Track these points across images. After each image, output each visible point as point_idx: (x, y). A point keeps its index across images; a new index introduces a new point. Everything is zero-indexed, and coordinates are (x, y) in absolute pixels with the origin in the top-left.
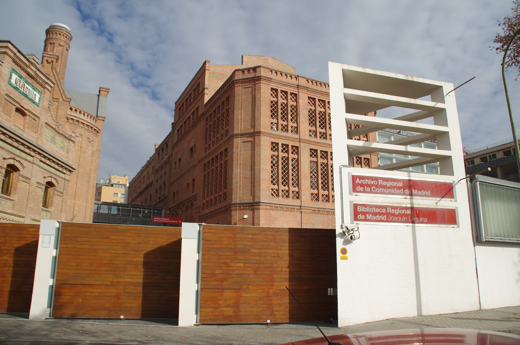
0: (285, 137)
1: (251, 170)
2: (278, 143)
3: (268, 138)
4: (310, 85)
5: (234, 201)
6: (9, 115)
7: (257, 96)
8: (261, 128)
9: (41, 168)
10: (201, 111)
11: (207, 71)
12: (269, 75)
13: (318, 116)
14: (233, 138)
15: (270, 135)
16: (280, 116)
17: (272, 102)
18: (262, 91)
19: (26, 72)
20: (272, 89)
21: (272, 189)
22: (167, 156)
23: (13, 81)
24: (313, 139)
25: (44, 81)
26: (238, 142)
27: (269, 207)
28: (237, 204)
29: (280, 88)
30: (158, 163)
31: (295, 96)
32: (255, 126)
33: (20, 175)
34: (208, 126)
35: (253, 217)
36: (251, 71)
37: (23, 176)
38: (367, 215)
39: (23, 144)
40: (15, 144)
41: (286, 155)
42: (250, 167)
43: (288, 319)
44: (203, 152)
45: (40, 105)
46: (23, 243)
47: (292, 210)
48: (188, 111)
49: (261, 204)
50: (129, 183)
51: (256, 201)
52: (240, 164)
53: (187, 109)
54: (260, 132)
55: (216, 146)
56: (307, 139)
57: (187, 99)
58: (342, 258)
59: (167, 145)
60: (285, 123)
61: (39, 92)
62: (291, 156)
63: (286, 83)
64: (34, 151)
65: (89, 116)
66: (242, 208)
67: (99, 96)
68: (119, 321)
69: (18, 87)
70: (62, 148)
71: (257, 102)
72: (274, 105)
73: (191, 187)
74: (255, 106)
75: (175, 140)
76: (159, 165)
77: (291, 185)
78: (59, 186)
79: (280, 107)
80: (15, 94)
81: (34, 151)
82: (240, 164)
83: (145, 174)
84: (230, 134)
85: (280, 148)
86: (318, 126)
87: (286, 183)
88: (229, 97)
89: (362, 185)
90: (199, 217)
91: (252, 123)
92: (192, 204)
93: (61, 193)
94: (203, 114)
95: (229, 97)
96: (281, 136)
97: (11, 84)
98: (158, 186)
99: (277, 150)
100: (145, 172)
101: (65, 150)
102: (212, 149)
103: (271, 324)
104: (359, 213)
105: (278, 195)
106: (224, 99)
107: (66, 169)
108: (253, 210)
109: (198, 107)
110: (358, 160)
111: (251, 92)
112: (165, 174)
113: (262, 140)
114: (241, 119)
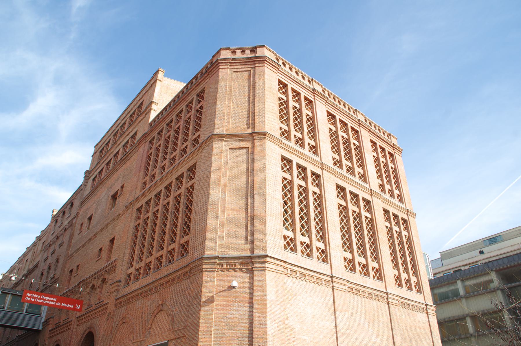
5: (208, 253)
7: (258, 83)
11: (158, 82)
18: (266, 77)
27: (281, 269)
28: (215, 258)
30: (53, 234)
47: (319, 281)
48: (117, 144)
49: (268, 259)
52: (225, 185)
66: (225, 266)
73: (104, 254)
74: (254, 96)
76: (54, 235)
82: (225, 185)
83: (29, 256)
92: (104, 280)
94: (146, 135)
100: (30, 254)
108: (251, 272)
111: (247, 77)
112: (61, 245)
113: (267, 146)
114: (229, 114)
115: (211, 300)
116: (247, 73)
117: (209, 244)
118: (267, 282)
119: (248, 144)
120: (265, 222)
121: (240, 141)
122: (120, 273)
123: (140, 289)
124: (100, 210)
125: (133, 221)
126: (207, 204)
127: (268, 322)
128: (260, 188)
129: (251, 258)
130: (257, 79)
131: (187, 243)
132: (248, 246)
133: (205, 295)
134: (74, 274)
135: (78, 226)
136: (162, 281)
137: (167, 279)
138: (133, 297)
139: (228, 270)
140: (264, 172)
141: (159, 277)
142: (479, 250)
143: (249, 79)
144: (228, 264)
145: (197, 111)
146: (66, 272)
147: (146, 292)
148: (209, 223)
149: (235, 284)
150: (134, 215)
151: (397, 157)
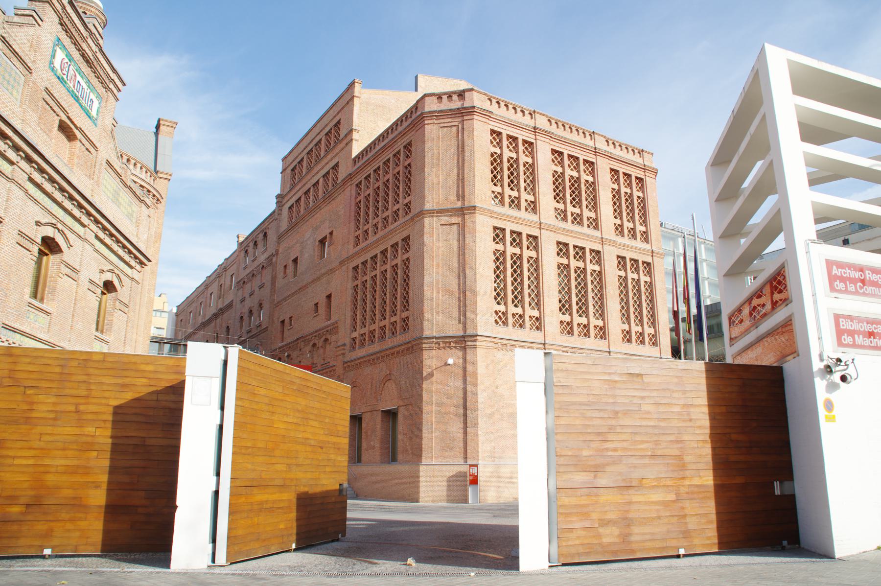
0: (516, 218)
1: (459, 276)
2: (504, 229)
3: (488, 219)
4: (553, 128)
5: (426, 334)
6: (48, 132)
7: (468, 142)
8: (476, 201)
9: (97, 251)
10: (342, 174)
12: (486, 105)
13: (568, 184)
14: (423, 218)
15: (491, 214)
16: (506, 181)
17: (492, 155)
18: (476, 133)
19: (80, 49)
20: (493, 132)
21: (496, 312)
22: (266, 255)
23: (57, 64)
24: (562, 225)
25: (108, 75)
26: (431, 224)
27: (493, 345)
28: (433, 338)
29: (506, 131)
30: (245, 268)
31: (529, 145)
32: (464, 196)
33: (63, 262)
34: (362, 198)
35: (465, 363)
36: (455, 97)
37: (68, 266)
38: (856, 336)
39: (71, 198)
40: (58, 195)
41: (517, 251)
42: (456, 271)
43: (717, 546)
44: (351, 246)
45: (99, 122)
46: (129, 396)
49: (478, 338)
50: (178, 307)
51: (469, 332)
52: (438, 265)
53: (310, 169)
54: (474, 208)
55: (381, 233)
56: (551, 223)
57: (311, 150)
58: (831, 419)
59: (265, 235)
60: (515, 194)
61: (99, 97)
62: (527, 254)
63: (515, 122)
64: (89, 214)
65: (144, 169)
66: (442, 345)
67: (157, 134)
68: (40, 561)
69: (65, 77)
70: (130, 216)
71: (467, 154)
72: (495, 160)
73: (322, 310)
75: (284, 225)
76: (248, 271)
77: (527, 305)
78: (123, 292)
79: (506, 165)
80: (59, 92)
81: (89, 214)
82: (438, 265)
84: (414, 210)
85: (508, 239)
86: (568, 201)
87: (518, 300)
88: (410, 144)
89: (842, 279)
90: (344, 363)
91: (458, 191)
92: (326, 340)
93: (126, 306)
94: (350, 176)
95: (410, 144)
96: (508, 216)
97: (53, 69)
98: (246, 311)
99: (503, 240)
101: (134, 220)
102: (372, 239)
103: (685, 556)
104: (845, 330)
105: (505, 323)
106: (399, 146)
107: (136, 257)
108: (464, 349)
109: (337, 165)
110: (632, 265)
111: (455, 135)
114: (438, 184)
115: (431, 375)
116: (455, 128)
117: (426, 325)
118: (478, 358)
119: (458, 220)
120: (476, 303)
121: (450, 216)
122: (344, 335)
123: (368, 356)
124: (307, 255)
125: (350, 280)
126: (422, 285)
127: (479, 393)
128: (471, 268)
129: (463, 337)
130: (466, 137)
131: (408, 259)
132: (461, 325)
133: (426, 371)
134: (287, 327)
135: (280, 268)
136: (387, 352)
137: (392, 351)
138: (361, 363)
139: (444, 348)
140: (474, 250)
141: (385, 347)
142: (843, 238)
143: (458, 137)
144: (444, 343)
145: (406, 167)
146: (276, 321)
147: (374, 360)
148: (425, 304)
149: (450, 361)
150: (351, 274)
151: (649, 181)
